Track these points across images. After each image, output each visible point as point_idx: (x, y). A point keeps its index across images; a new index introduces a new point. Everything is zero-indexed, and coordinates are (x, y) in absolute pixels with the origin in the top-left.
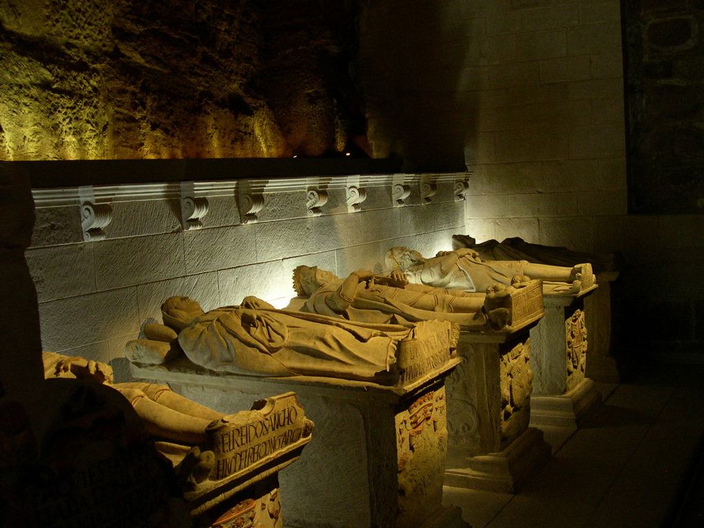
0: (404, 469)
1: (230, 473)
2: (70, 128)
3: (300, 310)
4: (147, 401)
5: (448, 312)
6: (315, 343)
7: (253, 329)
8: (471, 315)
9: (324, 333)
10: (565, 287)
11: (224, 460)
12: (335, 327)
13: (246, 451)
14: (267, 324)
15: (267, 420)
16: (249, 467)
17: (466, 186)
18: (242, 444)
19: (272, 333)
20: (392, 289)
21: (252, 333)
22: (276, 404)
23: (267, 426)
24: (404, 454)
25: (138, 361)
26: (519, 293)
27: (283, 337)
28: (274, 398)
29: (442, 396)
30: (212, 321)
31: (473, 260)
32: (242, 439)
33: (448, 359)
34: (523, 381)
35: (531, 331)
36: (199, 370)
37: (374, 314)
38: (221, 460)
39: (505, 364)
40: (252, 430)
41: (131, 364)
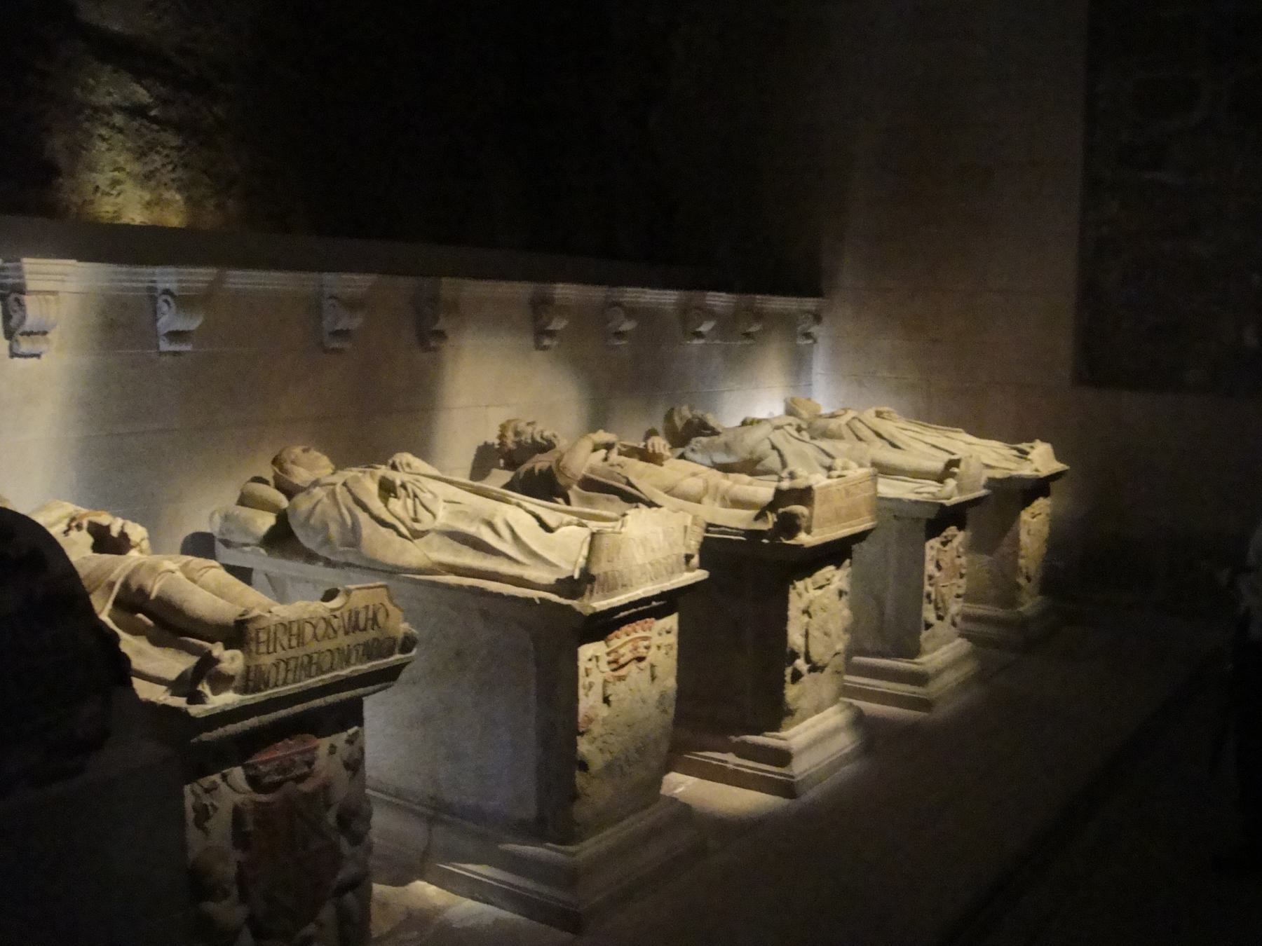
1: (267, 686)
2: (173, 180)
8: (753, 513)
9: (494, 515)
10: (928, 490)
13: (297, 658)
14: (416, 496)
17: (818, 318)
19: (420, 509)
20: (642, 465)
21: (390, 506)
25: (227, 537)
26: (828, 486)
31: (796, 434)
32: (290, 640)
35: (855, 547)
36: (311, 557)
39: (800, 595)
40: (308, 630)
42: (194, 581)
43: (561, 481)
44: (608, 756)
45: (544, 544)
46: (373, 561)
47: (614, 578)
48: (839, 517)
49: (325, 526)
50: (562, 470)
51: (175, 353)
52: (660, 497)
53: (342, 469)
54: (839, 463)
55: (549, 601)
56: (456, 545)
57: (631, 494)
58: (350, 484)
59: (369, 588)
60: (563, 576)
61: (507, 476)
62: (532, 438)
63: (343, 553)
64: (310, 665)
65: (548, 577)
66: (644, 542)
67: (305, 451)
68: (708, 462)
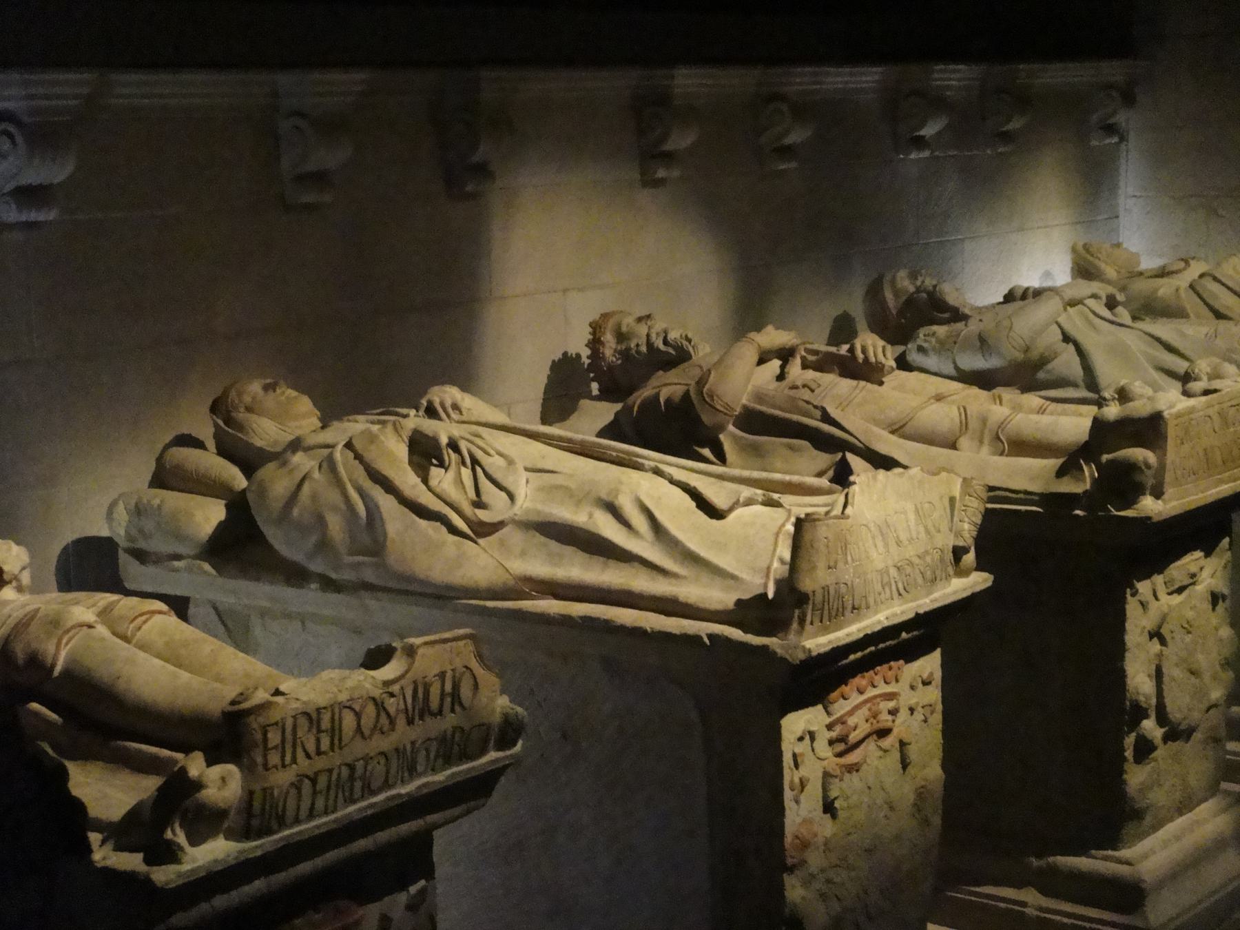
0: (803, 862)
1: (282, 824)
3: (600, 434)
4: (103, 639)
5: (994, 454)
6: (591, 516)
7: (435, 472)
8: (1053, 463)
9: (616, 492)
11: (264, 790)
12: (650, 475)
13: (330, 771)
14: (475, 462)
15: (392, 695)
16: (339, 814)
17: (1129, 99)
18: (319, 753)
20: (846, 384)
21: (433, 482)
22: (418, 658)
23: (392, 711)
24: (805, 821)
25: (141, 544)
26: (1192, 410)
27: (511, 497)
28: (417, 641)
29: (931, 674)
30: (332, 446)
31: (1106, 313)
32: (318, 741)
33: (948, 578)
34: (1200, 657)
35: (1001, 300)
36: (296, 575)
37: (791, 448)
38: (257, 787)
40: (349, 720)
41: (121, 552)
42: (126, 639)
43: (706, 418)
44: (836, 907)
45: (713, 536)
46: (411, 579)
47: (840, 597)
48: (1210, 465)
49: (321, 521)
50: (708, 401)
51: (30, 225)
52: (888, 445)
53: (339, 418)
54: (1203, 366)
55: (728, 641)
56: (554, 545)
57: (832, 437)
58: (358, 444)
59: (445, 641)
60: (746, 596)
61: (606, 412)
62: (650, 344)
63: (356, 566)
64: (354, 781)
65: (719, 597)
66: (884, 529)
67: (266, 388)
68: (949, 369)
